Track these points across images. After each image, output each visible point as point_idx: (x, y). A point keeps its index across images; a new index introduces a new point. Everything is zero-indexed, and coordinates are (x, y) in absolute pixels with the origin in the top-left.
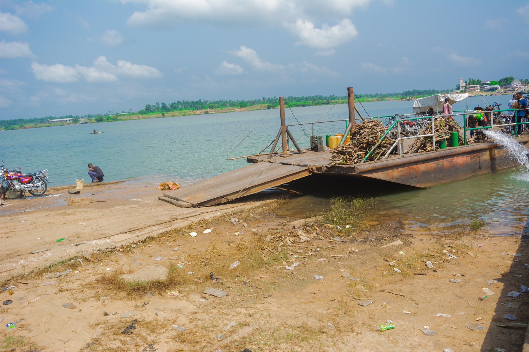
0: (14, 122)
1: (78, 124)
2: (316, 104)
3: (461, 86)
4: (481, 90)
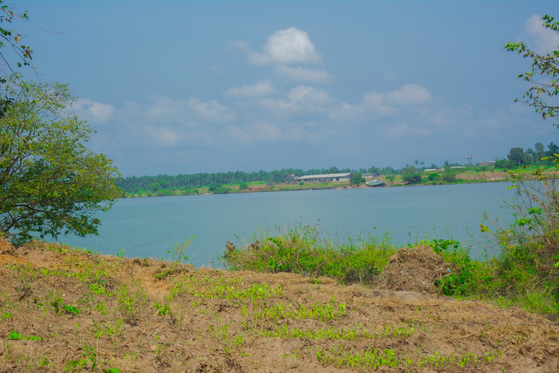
0: (225, 178)
1: (363, 185)
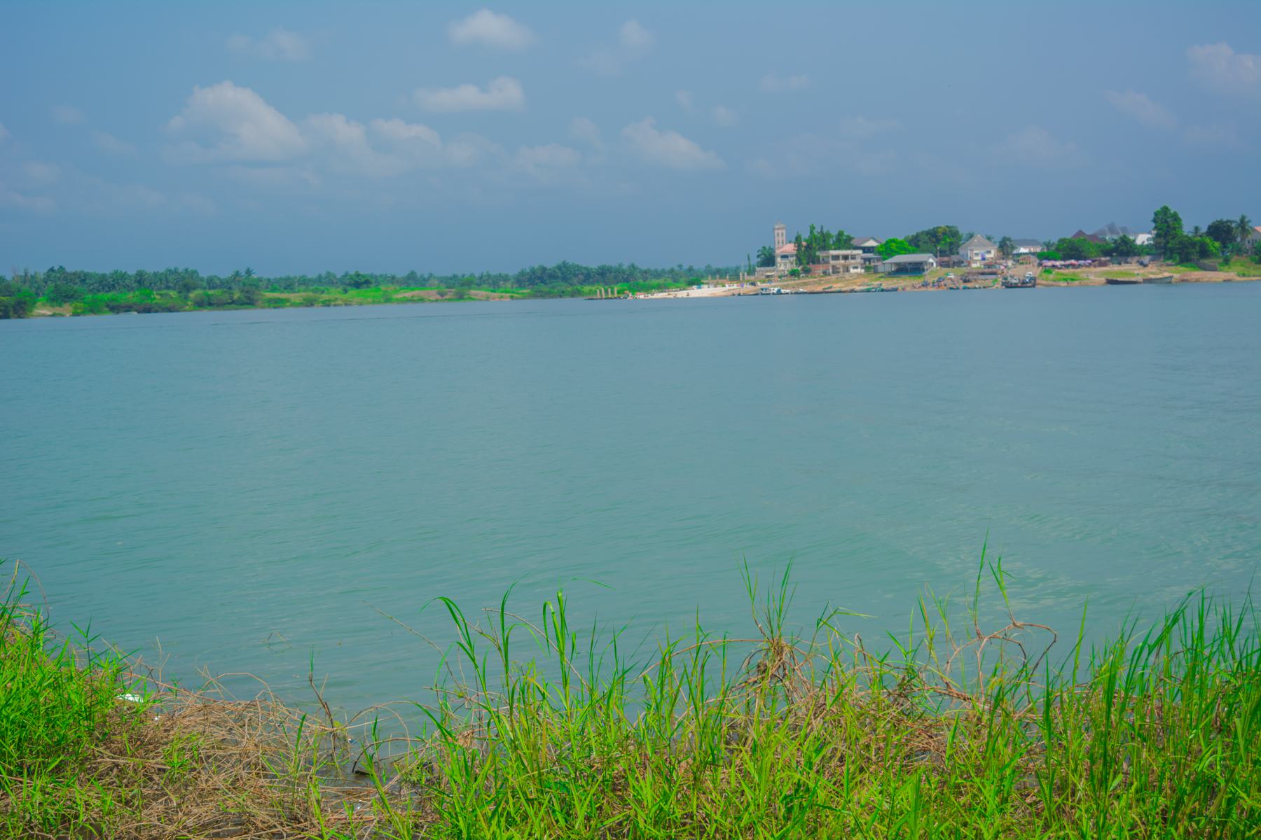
2: (201, 304)
3: (778, 252)
4: (867, 269)
